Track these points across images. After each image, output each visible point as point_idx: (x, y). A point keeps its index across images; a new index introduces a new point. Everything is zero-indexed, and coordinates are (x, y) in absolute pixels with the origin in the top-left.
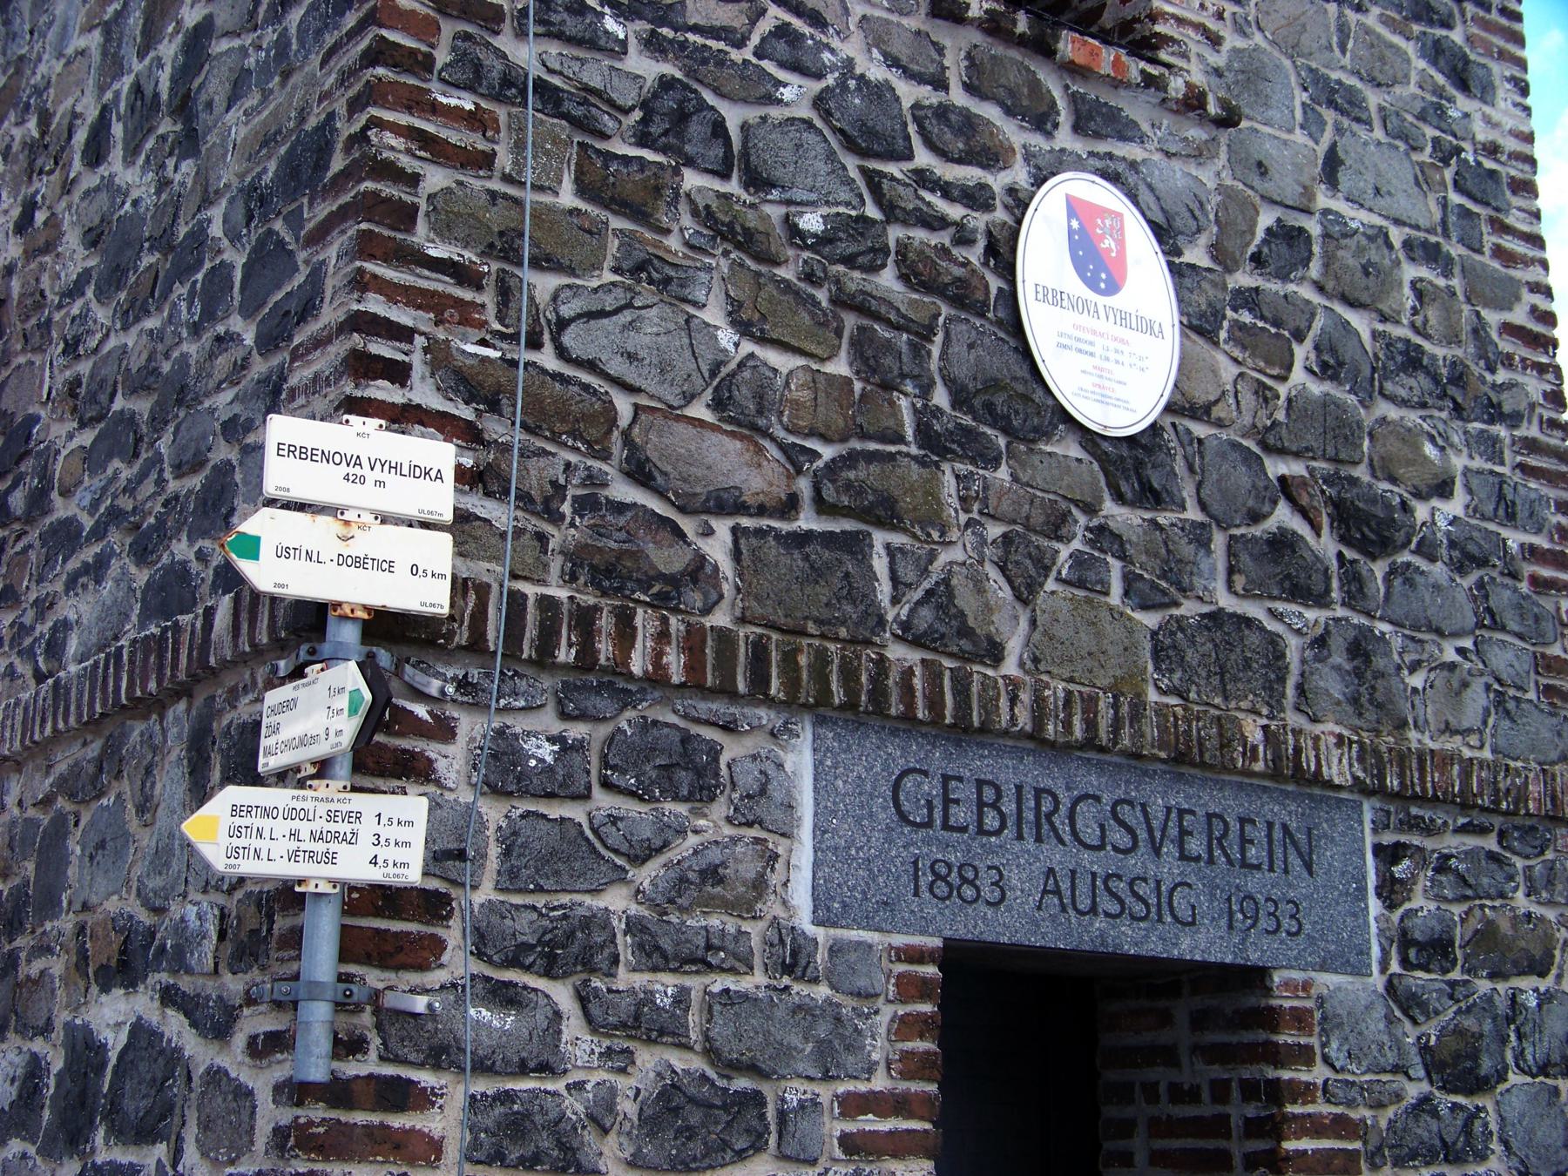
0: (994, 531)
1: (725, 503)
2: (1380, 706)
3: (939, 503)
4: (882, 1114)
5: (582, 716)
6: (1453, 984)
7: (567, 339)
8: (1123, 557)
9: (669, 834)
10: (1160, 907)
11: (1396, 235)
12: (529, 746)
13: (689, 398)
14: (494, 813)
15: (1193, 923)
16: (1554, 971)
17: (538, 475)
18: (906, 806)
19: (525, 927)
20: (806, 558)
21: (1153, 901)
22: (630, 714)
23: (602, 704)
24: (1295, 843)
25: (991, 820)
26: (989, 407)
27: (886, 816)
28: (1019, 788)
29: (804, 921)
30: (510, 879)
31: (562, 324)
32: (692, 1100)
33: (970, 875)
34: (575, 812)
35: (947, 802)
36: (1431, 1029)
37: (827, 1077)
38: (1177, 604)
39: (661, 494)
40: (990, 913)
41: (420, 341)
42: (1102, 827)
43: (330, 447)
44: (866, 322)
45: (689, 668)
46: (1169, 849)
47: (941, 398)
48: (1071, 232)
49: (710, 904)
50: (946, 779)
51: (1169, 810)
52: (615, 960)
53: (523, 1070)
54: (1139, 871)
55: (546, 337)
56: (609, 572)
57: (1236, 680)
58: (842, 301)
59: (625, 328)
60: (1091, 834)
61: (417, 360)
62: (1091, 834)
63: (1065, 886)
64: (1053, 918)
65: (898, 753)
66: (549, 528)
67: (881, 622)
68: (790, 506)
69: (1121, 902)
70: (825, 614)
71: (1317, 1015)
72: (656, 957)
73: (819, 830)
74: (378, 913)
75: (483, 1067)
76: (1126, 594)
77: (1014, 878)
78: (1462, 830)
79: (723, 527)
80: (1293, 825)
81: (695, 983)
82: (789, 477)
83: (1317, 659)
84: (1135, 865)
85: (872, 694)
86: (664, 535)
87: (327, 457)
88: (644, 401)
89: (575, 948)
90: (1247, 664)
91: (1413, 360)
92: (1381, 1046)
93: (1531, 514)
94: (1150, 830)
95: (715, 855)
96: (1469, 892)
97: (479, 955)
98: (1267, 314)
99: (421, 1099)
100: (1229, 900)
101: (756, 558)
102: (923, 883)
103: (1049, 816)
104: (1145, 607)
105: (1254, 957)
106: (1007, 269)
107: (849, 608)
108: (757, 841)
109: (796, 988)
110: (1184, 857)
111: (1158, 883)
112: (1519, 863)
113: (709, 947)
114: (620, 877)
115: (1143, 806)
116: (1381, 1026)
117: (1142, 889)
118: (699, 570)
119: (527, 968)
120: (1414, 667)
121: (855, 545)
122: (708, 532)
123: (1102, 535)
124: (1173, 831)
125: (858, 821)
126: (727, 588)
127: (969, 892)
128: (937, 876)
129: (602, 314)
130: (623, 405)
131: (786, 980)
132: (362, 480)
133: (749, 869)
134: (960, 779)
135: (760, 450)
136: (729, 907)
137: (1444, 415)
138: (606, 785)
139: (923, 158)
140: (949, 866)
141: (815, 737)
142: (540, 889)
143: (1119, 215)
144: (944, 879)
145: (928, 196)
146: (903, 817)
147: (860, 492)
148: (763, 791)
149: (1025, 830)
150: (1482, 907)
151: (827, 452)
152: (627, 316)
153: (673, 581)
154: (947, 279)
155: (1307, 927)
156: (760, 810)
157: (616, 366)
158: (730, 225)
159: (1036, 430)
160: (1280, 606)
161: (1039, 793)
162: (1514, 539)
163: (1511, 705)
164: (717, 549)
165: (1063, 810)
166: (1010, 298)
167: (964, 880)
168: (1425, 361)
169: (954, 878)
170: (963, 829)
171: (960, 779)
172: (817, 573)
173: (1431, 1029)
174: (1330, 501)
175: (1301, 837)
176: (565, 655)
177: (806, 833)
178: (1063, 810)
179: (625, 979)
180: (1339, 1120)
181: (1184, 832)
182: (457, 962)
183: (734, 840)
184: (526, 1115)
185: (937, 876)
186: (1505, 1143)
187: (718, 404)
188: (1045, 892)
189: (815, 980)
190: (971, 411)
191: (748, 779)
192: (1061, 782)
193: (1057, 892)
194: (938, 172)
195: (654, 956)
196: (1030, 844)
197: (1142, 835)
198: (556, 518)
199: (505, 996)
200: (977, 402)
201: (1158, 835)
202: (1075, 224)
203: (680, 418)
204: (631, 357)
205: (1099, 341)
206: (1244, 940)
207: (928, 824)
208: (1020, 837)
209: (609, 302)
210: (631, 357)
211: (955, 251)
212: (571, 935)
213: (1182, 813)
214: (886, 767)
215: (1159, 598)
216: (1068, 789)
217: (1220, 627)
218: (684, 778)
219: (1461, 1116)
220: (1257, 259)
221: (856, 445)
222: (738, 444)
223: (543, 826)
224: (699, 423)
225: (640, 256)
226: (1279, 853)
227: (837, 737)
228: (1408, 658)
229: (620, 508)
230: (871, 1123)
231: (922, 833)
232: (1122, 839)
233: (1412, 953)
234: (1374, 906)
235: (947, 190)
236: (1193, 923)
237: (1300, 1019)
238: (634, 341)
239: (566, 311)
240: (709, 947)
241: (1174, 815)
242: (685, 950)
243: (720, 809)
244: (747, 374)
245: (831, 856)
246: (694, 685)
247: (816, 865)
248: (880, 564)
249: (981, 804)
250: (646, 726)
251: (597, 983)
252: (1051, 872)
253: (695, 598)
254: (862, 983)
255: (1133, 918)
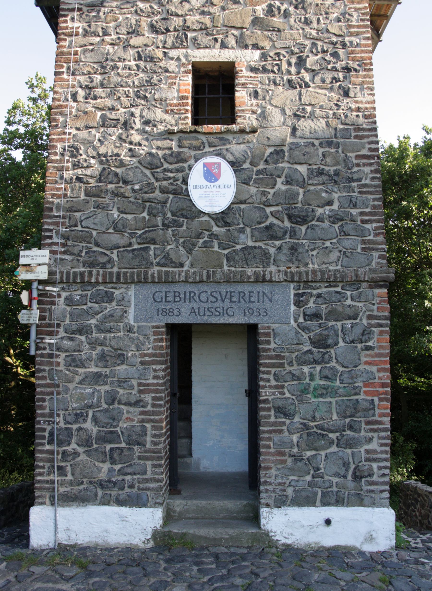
0: (181, 240)
1: (117, 247)
2: (299, 261)
3: (166, 237)
4: (150, 357)
5: (86, 290)
6: (320, 324)
7: (83, 224)
8: (218, 239)
9: (103, 309)
10: (225, 312)
11: (317, 143)
12: (75, 297)
13: (108, 229)
14: (69, 309)
15: (233, 316)
16: (359, 318)
17: (76, 250)
18: (156, 299)
19: (74, 328)
20: (133, 254)
21: (221, 312)
22: (95, 289)
23: (89, 288)
24: (267, 296)
25: (177, 299)
26: (182, 214)
27: (151, 300)
28: (185, 292)
29: (132, 322)
30: (72, 320)
31: (81, 221)
32: (107, 355)
33: (172, 310)
34: (84, 307)
35: (166, 297)
36: (312, 334)
37: (138, 350)
38: (235, 247)
39: (102, 248)
40: (176, 317)
41: (54, 231)
42: (208, 298)
43: (28, 255)
44: (151, 204)
45: (103, 279)
46: (227, 301)
47: (169, 215)
48: (204, 171)
49: (110, 321)
50: (166, 292)
51: (227, 292)
52: (92, 332)
53: (75, 351)
54: (218, 306)
55: (79, 224)
56: (91, 264)
57: (250, 261)
58: (145, 201)
59: (94, 219)
60: (204, 299)
61: (54, 235)
62: (204, 299)
63: (197, 311)
64: (193, 317)
65: (154, 288)
66: (80, 258)
67: (152, 263)
68: (130, 245)
69: (212, 313)
70: (138, 264)
71: (272, 333)
72: (101, 331)
73: (136, 305)
74: (47, 327)
75: (66, 351)
76: (219, 247)
77: (183, 310)
78: (326, 287)
79: (115, 251)
80: (266, 292)
81: (108, 335)
82: (130, 239)
83: (278, 253)
84: (216, 305)
85: (144, 278)
86: (103, 255)
87: (28, 256)
88: (98, 231)
89: (84, 331)
90: (255, 257)
91: (320, 173)
92: (292, 339)
93: (363, 204)
94: (221, 297)
95: (112, 312)
96: (328, 302)
97: (66, 332)
98: (268, 173)
99: (57, 356)
100: (245, 310)
101: (122, 256)
102: (160, 313)
103: (193, 297)
104: (224, 249)
105: (252, 322)
106: (186, 184)
107: (144, 262)
108: (121, 308)
109: (130, 334)
110: (231, 301)
111: (223, 308)
112: (349, 293)
113: (111, 328)
114: (93, 317)
115: (220, 293)
116: (294, 335)
117: (218, 309)
118: (110, 261)
119: (76, 334)
120: (312, 250)
121: (146, 249)
122: (112, 253)
123: (212, 236)
124: (228, 296)
125: (144, 303)
126: (116, 263)
127: (171, 314)
128: (163, 311)
129: (90, 217)
130: (94, 233)
131: (128, 333)
132: (33, 259)
133: (119, 314)
134: (170, 292)
135: (123, 235)
136: (114, 321)
137: (332, 184)
138: (90, 302)
139: (166, 165)
140: (166, 309)
141: (135, 288)
142: (77, 321)
143: (220, 163)
144: (165, 312)
145: (166, 174)
146: (155, 301)
147: (147, 239)
148: (123, 299)
149: (186, 300)
150: (332, 305)
151: (140, 232)
152: (94, 216)
153: (105, 263)
154: (171, 190)
155: (269, 314)
156: (122, 303)
157: (92, 226)
158: (117, 193)
159: (193, 216)
160: (267, 242)
161: (190, 293)
162: (354, 212)
163: (349, 254)
164: (115, 256)
165: (197, 295)
166: (187, 189)
167: (170, 312)
168: (325, 172)
169: (168, 311)
170: (170, 302)
171: (170, 292)
172: (136, 257)
173: (312, 334)
174: (286, 214)
175: (269, 294)
176: (79, 281)
177: (133, 306)
178: (197, 295)
179: (94, 335)
180: (277, 356)
181: (231, 297)
182: (62, 333)
183: (116, 309)
184: (75, 359)
185: (163, 311)
186: (337, 359)
187: (114, 229)
188: (191, 312)
189: (134, 333)
190: (177, 216)
191: (120, 297)
192: (196, 290)
193: (195, 312)
194: (169, 167)
195: (100, 330)
196: (187, 303)
197: (219, 298)
198: (81, 256)
199: (71, 339)
200: (178, 214)
201: (224, 298)
202: (205, 169)
203: (105, 233)
204: (95, 224)
205: (211, 194)
206: (248, 318)
207: (162, 301)
208: (185, 302)
209: (91, 215)
210: (95, 224)
211: (174, 183)
212: (83, 328)
213: (231, 292)
214: (151, 292)
215: (227, 247)
216: (198, 290)
217: (247, 250)
218: (106, 299)
219: (321, 355)
220: (266, 161)
221: (147, 229)
222: (119, 235)
223: (78, 310)
224: (110, 233)
225: (97, 204)
226: (261, 298)
227: (140, 287)
228: (310, 248)
229: (94, 252)
230: (147, 359)
231: (160, 303)
232: (214, 300)
233: (306, 317)
234: (293, 308)
235: (171, 171)
236: (233, 316)
237: (267, 335)
238: (96, 221)
239: (82, 218)
240: (111, 328)
241: (229, 293)
242: (106, 329)
243: (114, 303)
244: (120, 221)
245: (138, 310)
246: (104, 282)
247: (135, 312)
248: (152, 253)
249: (175, 296)
250: (98, 290)
251: (89, 336)
252: (193, 308)
253: (109, 266)
254: (145, 333)
255: (215, 316)
